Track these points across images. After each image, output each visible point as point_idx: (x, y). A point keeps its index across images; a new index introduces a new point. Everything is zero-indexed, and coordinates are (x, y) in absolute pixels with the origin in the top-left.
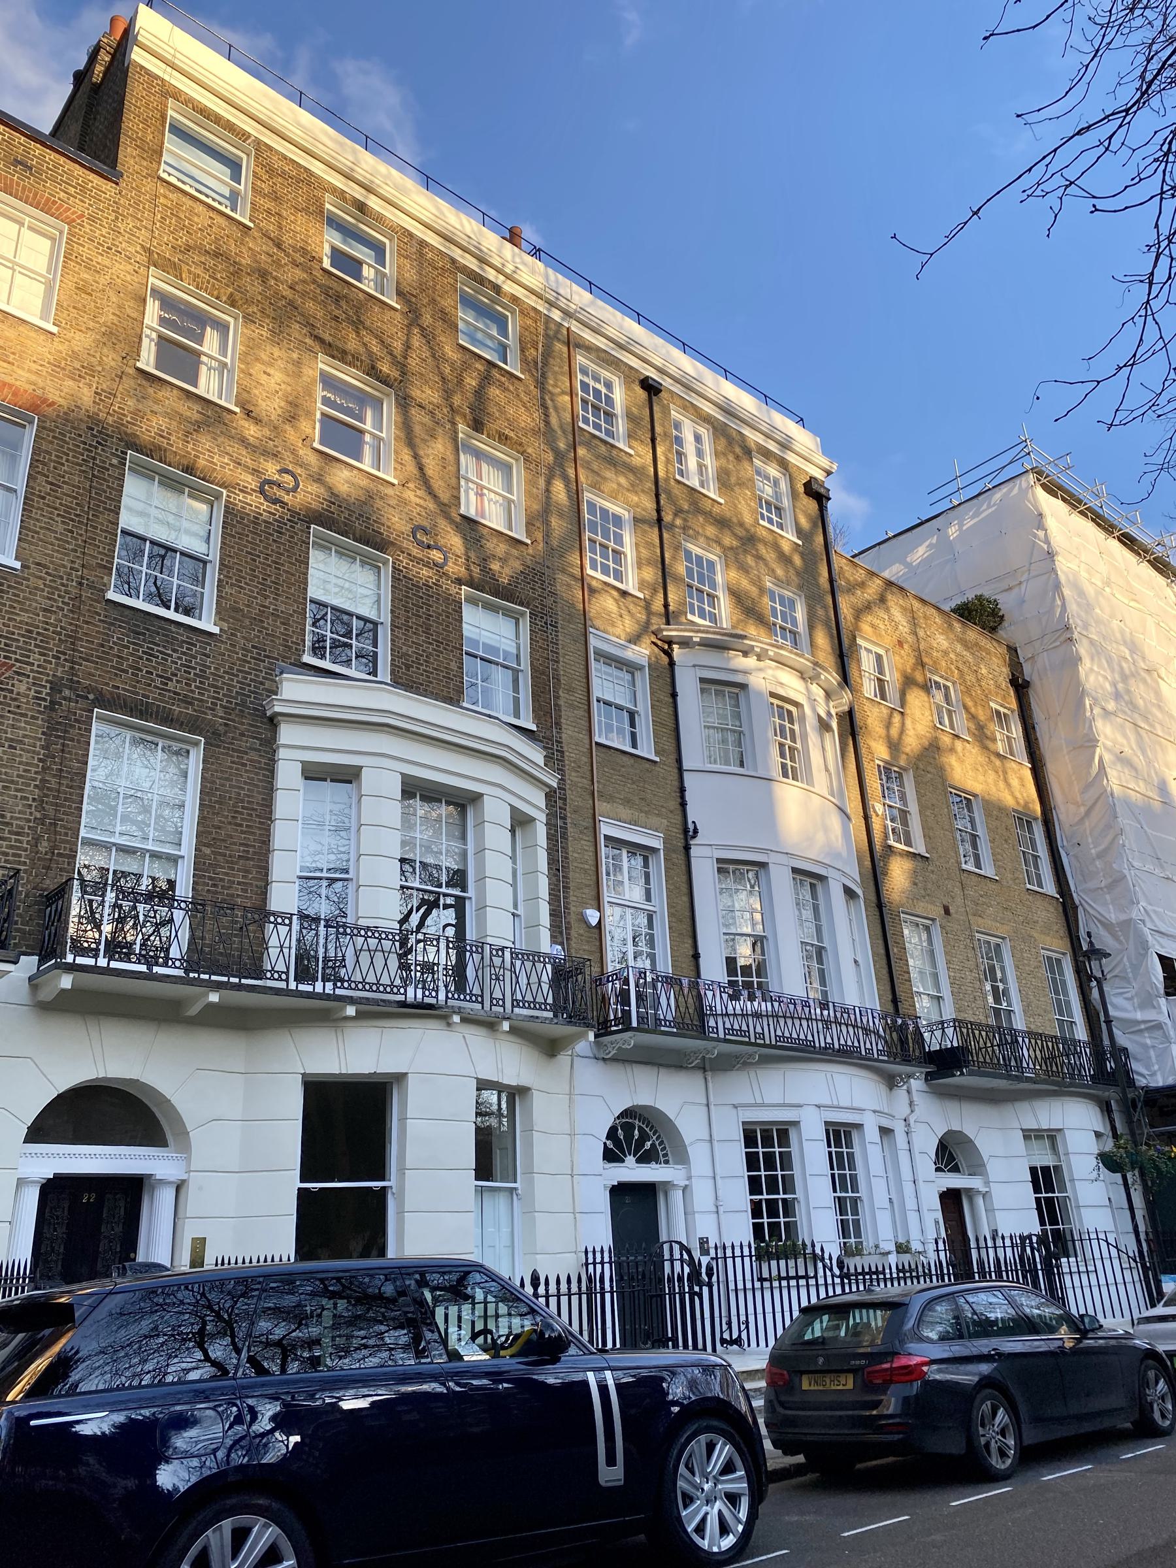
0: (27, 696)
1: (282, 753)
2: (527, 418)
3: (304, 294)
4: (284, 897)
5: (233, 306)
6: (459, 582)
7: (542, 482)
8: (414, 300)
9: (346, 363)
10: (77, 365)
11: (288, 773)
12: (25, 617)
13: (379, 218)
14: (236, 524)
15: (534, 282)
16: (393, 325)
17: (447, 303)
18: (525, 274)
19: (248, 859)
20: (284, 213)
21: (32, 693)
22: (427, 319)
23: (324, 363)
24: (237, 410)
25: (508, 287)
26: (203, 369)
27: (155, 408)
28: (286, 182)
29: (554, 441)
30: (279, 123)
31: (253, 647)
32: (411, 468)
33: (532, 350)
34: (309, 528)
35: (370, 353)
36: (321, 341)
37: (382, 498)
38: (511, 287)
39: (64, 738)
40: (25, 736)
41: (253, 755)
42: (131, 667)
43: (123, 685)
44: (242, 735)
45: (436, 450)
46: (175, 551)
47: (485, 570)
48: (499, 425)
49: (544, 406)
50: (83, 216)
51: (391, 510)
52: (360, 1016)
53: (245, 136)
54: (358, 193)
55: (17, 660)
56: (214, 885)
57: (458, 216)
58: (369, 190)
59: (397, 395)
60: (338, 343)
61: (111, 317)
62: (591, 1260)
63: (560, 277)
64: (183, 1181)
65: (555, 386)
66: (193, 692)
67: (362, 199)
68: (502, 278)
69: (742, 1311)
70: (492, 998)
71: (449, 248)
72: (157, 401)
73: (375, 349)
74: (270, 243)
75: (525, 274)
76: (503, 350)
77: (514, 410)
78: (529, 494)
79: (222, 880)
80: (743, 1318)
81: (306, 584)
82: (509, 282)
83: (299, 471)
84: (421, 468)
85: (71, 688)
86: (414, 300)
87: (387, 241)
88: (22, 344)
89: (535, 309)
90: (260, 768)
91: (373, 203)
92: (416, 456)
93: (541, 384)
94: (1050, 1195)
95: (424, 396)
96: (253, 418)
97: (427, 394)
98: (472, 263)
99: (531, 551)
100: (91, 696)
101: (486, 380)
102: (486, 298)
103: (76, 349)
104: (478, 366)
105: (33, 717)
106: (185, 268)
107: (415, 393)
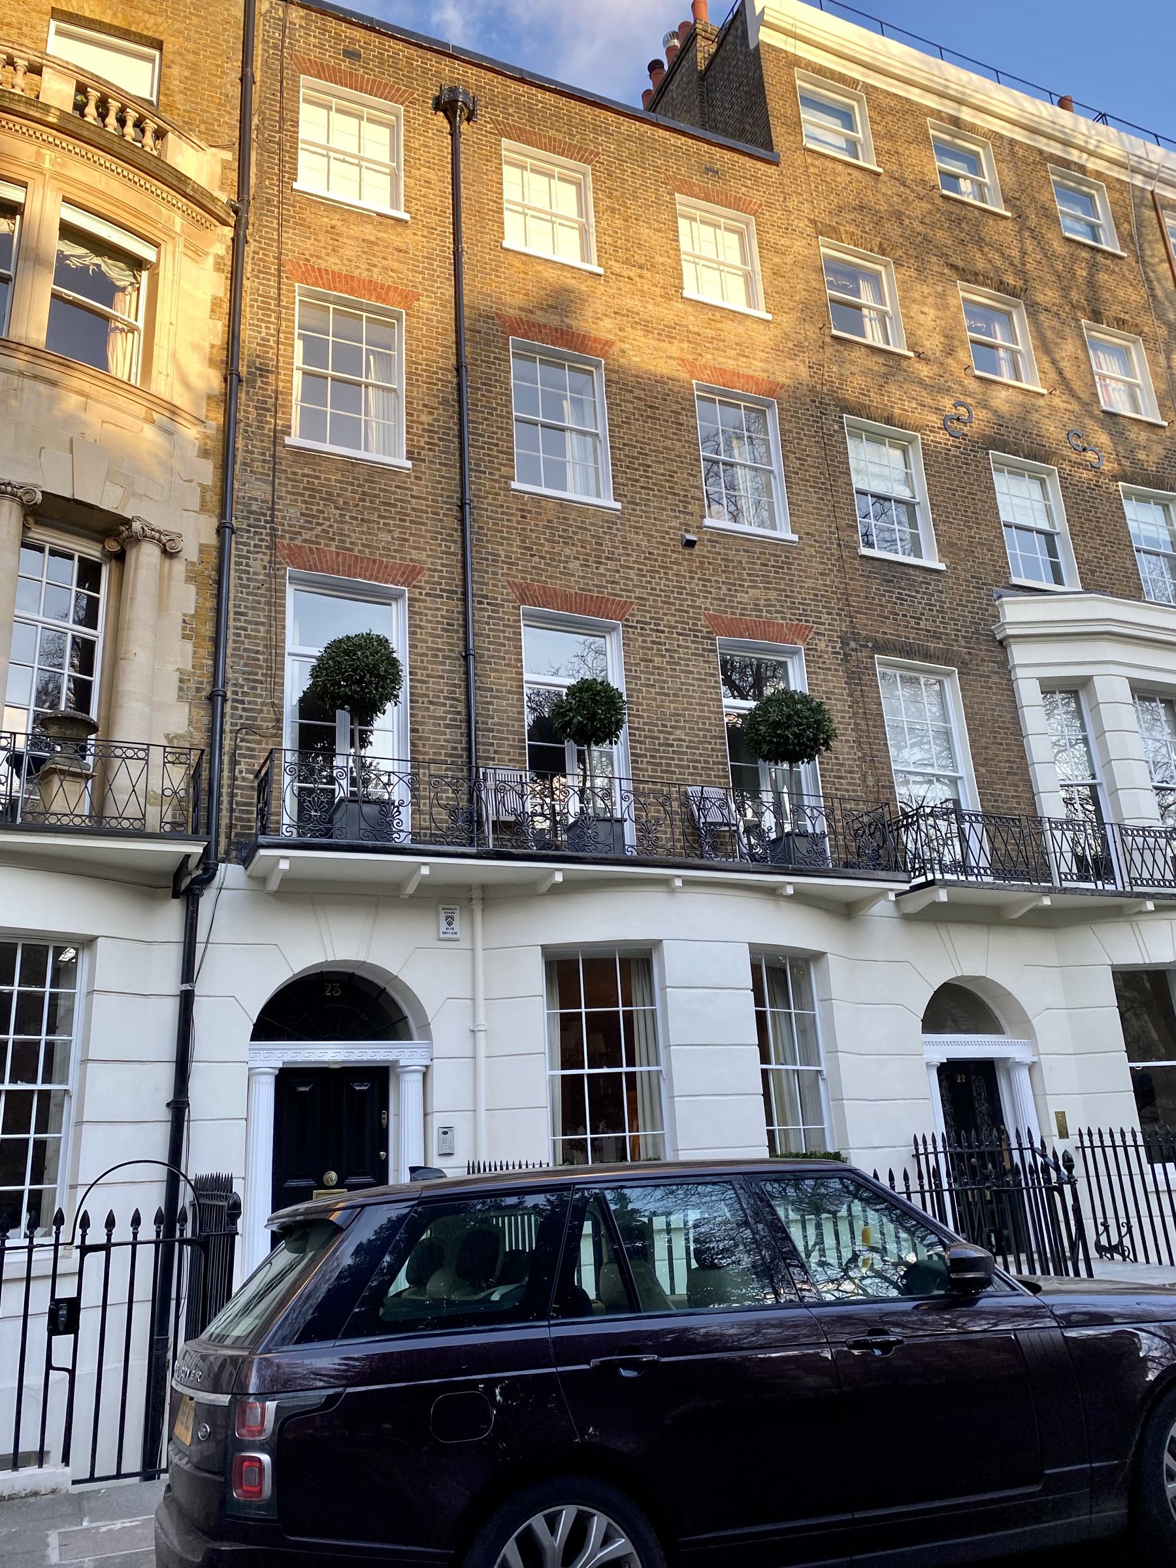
0: (827, 652)
1: (1019, 673)
2: (1135, 296)
3: (932, 226)
4: (1052, 806)
5: (883, 255)
6: (1115, 478)
7: (1162, 358)
8: (1018, 203)
9: (979, 285)
10: (791, 345)
11: (1028, 691)
12: (809, 583)
13: (973, 128)
14: (936, 464)
15: (1111, 150)
16: (1005, 233)
17: (1044, 197)
18: (1105, 144)
19: (1014, 774)
20: (901, 150)
21: (830, 649)
22: (1033, 220)
23: (963, 292)
24: (911, 354)
25: (1092, 164)
26: (867, 321)
27: (854, 369)
28: (895, 117)
29: (1164, 314)
30: (882, 61)
31: (973, 577)
32: (1053, 376)
33: (1126, 225)
34: (987, 454)
35: (997, 269)
36: (953, 267)
37: (1037, 411)
38: (1094, 163)
39: (860, 684)
40: (834, 687)
41: (995, 678)
42: (891, 613)
43: (887, 631)
44: (983, 660)
45: (1068, 348)
46: (866, 494)
47: (1135, 462)
48: (1114, 310)
49: (1148, 280)
50: (761, 204)
51: (1047, 421)
52: (1159, 909)
53: (854, 83)
54: (949, 108)
55: (814, 622)
56: (996, 801)
57: (1034, 104)
58: (960, 102)
59: (1026, 305)
60: (968, 267)
61: (804, 293)
62: (1087, 1143)
63: (1133, 138)
64: (1034, 1063)
65: (1153, 256)
66: (938, 627)
67: (954, 113)
68: (1085, 156)
69: (1122, 1213)
70: (1060, 874)
71: (1035, 140)
72: (852, 362)
73: (999, 263)
74: (897, 184)
75: (1105, 144)
76: (1093, 230)
77: (1123, 293)
78: (1155, 375)
79: (1000, 795)
80: (1123, 1220)
81: (997, 508)
82: (1092, 159)
83: (969, 400)
84: (1060, 373)
85: (855, 640)
86: (1018, 203)
87: (855, 104)
88: (751, 337)
89: (1118, 180)
90: (1003, 690)
91: (966, 115)
92: (1054, 362)
93: (1140, 259)
94: (21, 1086)
95: (1047, 298)
96: (924, 359)
97: (1047, 295)
98: (1056, 149)
99: (1168, 434)
100: (870, 645)
101: (1093, 267)
102: (1075, 179)
103: (786, 330)
104: (1084, 254)
105: (836, 670)
106: (842, 229)
107: (1040, 298)
